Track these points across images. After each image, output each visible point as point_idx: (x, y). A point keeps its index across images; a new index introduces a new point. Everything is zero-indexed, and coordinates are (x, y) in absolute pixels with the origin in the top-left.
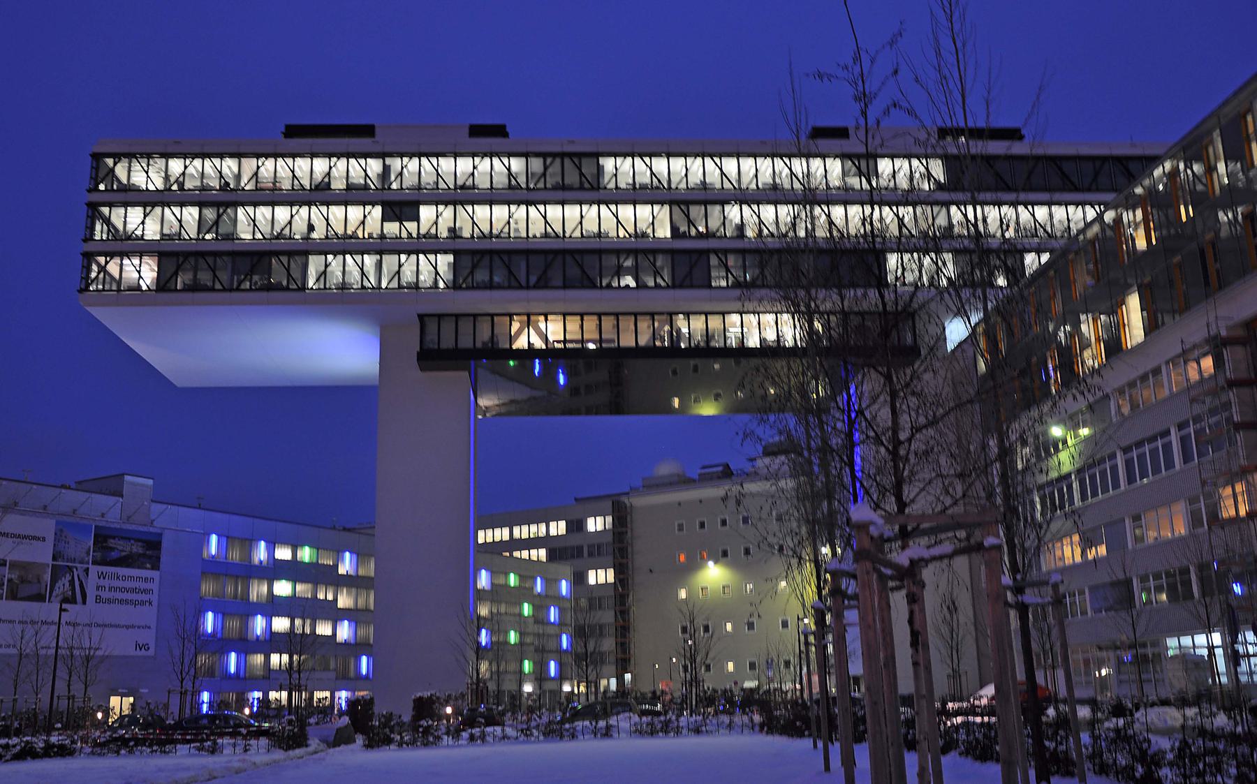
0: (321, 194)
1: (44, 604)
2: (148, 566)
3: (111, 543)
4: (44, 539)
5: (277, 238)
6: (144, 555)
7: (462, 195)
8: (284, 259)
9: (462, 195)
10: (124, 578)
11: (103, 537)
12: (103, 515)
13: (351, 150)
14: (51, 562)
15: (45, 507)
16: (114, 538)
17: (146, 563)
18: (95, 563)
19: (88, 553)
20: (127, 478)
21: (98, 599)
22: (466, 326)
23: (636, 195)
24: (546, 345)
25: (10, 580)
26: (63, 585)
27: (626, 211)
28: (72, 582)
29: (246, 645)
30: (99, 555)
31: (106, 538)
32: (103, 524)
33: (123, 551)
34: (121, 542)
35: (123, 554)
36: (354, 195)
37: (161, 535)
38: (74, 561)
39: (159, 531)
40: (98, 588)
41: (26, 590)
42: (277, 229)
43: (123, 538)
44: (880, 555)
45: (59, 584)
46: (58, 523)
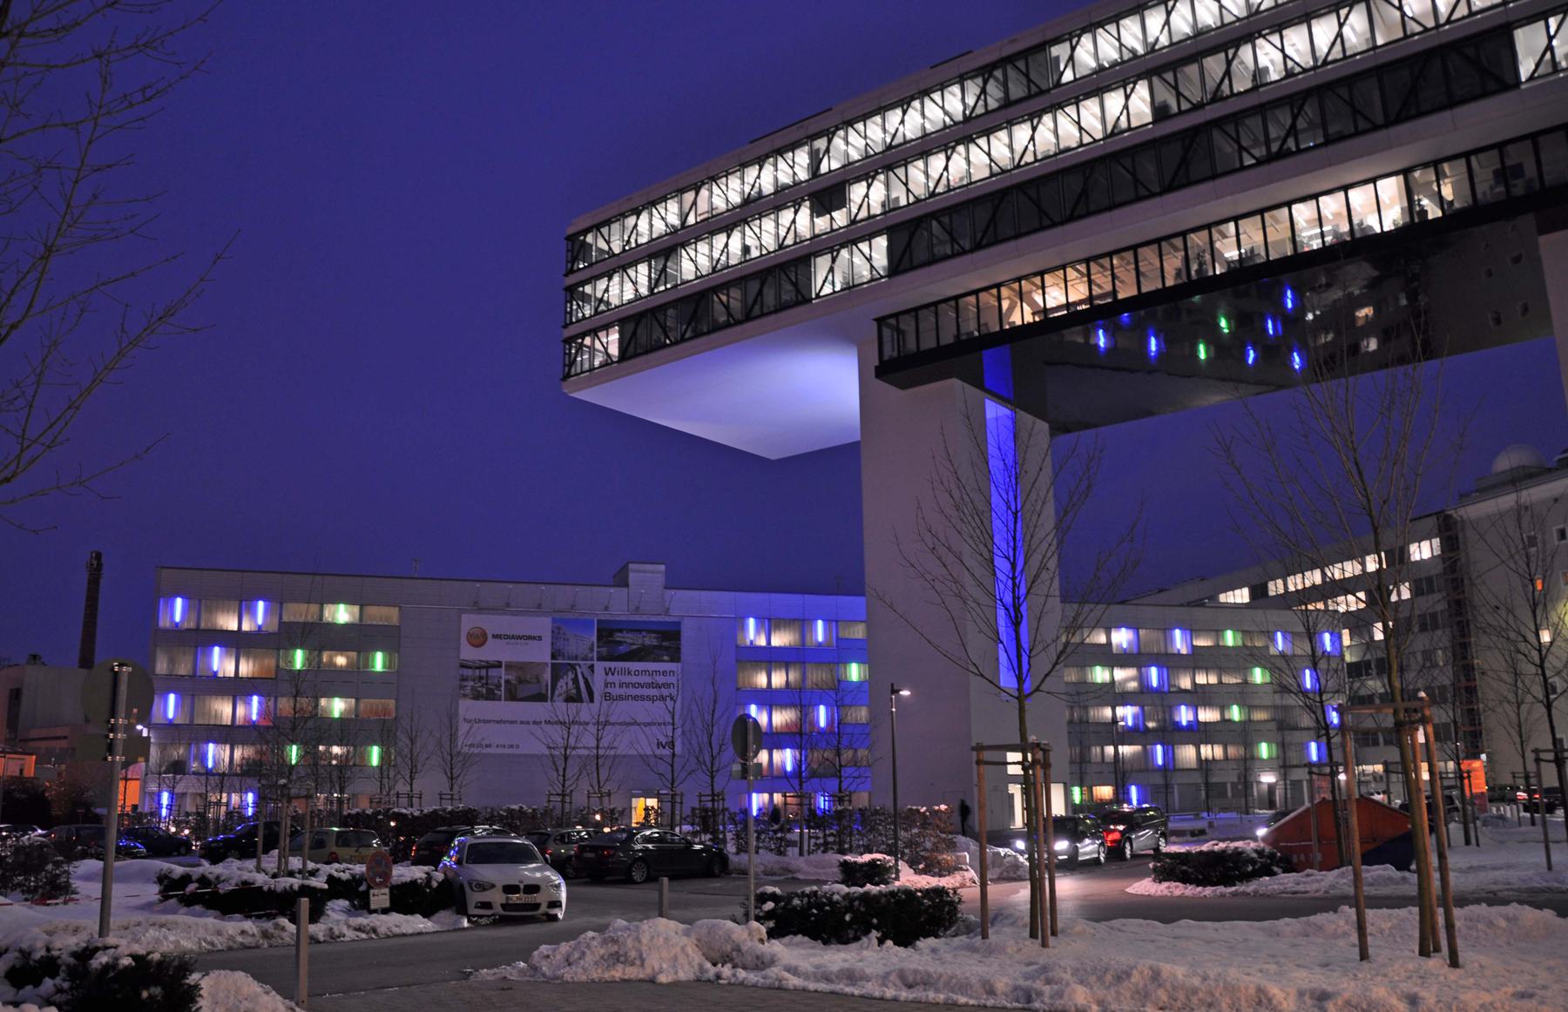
0: (752, 208)
1: (544, 704)
2: (666, 658)
3: (618, 637)
4: (540, 638)
5: (1113, 134)
6: (659, 647)
7: (893, 159)
8: (1127, 162)
9: (893, 159)
10: (637, 673)
11: (607, 632)
12: (606, 608)
13: (777, 145)
14: (548, 659)
15: (539, 606)
16: (621, 631)
17: (663, 655)
18: (599, 659)
19: (592, 650)
20: (631, 566)
21: (607, 697)
22: (928, 319)
23: (1098, 83)
24: (1442, 209)
25: (507, 682)
26: (565, 684)
27: (1090, 108)
28: (575, 680)
29: (1172, 734)
30: (604, 650)
31: (611, 632)
32: (608, 618)
33: (634, 644)
34: (630, 635)
35: (634, 647)
36: (784, 198)
37: (678, 624)
38: (576, 658)
39: (676, 620)
40: (606, 686)
41: (523, 691)
42: (1211, 85)
43: (632, 631)
44: (152, 740)
45: (561, 683)
46: (554, 621)
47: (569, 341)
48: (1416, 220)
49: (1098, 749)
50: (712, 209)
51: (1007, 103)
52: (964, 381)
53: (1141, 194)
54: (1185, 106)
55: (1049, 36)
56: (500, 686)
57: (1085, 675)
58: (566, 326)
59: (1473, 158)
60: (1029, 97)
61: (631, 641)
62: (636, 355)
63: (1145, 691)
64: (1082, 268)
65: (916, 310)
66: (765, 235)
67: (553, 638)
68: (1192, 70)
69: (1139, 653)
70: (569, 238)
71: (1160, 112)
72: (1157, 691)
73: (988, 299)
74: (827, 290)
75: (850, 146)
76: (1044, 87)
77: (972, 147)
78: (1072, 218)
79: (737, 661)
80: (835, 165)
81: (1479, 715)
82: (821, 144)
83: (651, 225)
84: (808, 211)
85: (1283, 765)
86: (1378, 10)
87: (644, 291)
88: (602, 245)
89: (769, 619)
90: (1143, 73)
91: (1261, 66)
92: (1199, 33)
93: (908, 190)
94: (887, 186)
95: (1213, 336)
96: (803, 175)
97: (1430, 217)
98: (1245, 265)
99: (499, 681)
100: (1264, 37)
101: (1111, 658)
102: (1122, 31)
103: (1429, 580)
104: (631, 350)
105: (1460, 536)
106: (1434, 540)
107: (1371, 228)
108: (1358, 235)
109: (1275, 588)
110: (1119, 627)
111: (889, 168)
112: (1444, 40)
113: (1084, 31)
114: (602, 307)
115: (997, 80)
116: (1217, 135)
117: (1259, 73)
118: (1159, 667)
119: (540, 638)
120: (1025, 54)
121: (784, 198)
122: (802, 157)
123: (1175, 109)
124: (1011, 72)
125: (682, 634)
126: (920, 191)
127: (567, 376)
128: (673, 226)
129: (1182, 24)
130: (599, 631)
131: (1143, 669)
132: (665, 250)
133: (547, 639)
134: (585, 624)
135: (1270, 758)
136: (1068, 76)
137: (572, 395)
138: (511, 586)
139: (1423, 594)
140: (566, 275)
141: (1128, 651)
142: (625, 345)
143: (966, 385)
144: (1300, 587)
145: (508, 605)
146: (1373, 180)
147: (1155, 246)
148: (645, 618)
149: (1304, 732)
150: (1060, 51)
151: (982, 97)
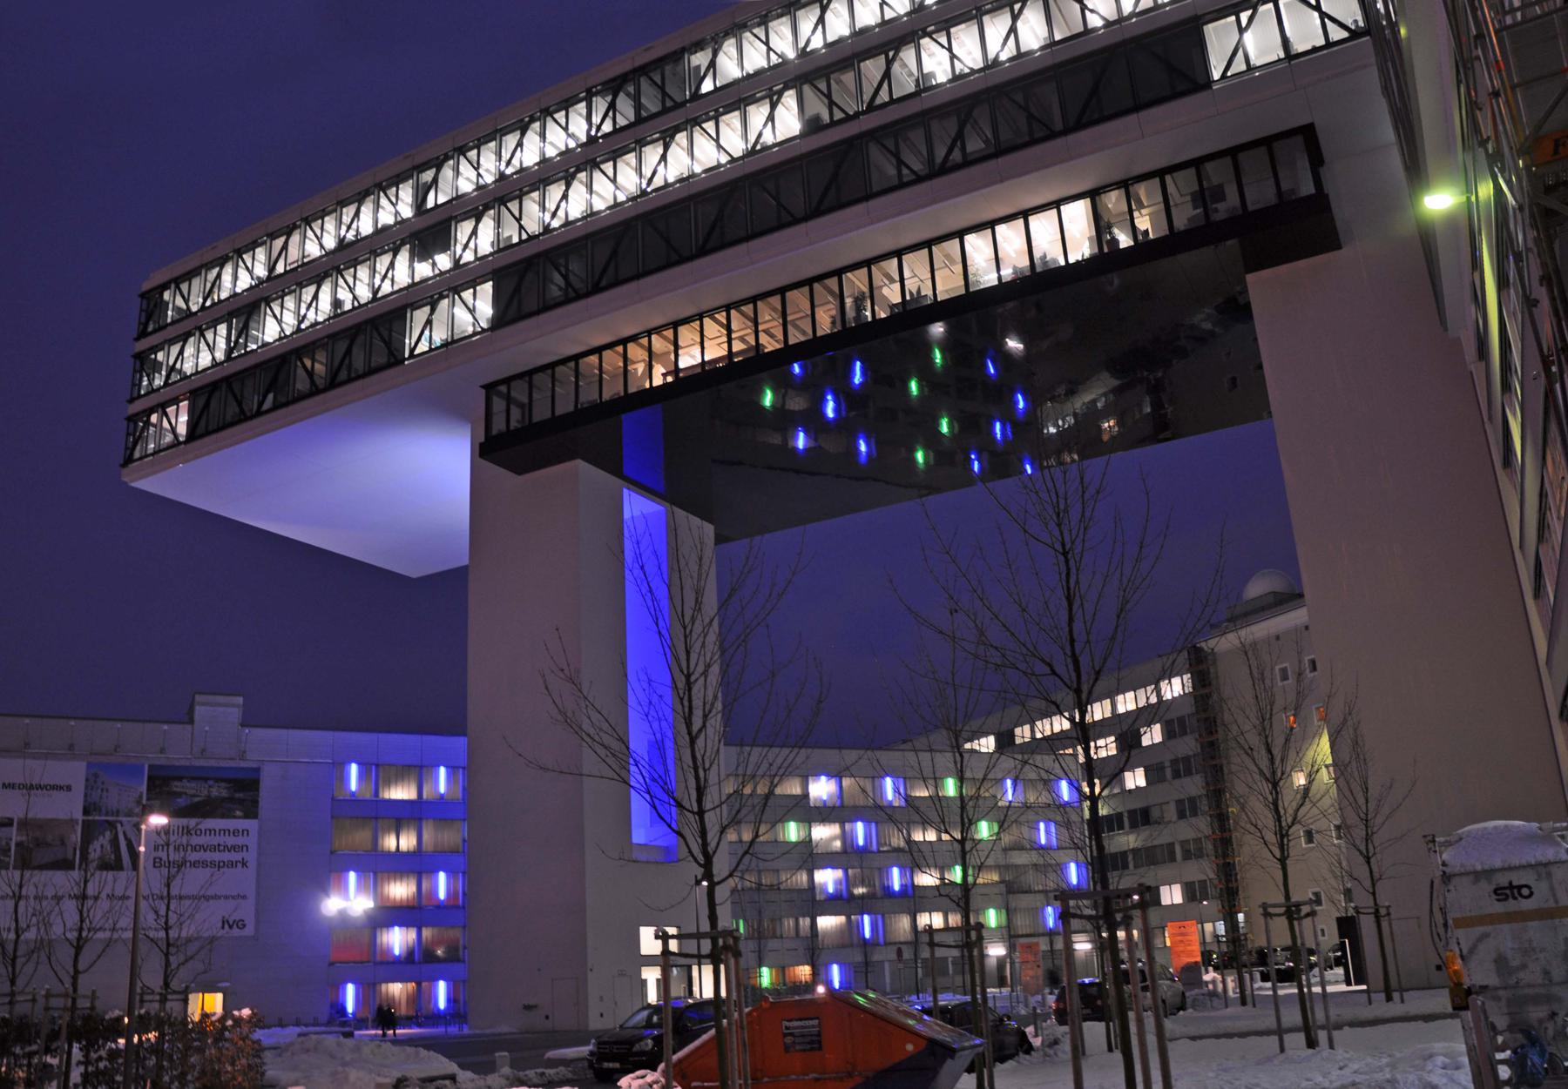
0: (348, 255)
2: (238, 813)
4: (69, 788)
6: (231, 799)
15: (71, 747)
16: (180, 779)
23: (738, 96)
31: (167, 780)
34: (193, 785)
35: (197, 799)
37: (257, 770)
39: (255, 766)
46: (90, 765)
47: (132, 419)
48: (1106, 250)
49: (792, 922)
50: (304, 257)
51: (639, 121)
52: (687, 511)
53: (786, 220)
54: (838, 115)
55: (686, 42)
56: (9, 850)
57: (776, 834)
58: (131, 401)
59: (1168, 178)
60: (665, 111)
61: (193, 792)
62: (208, 433)
63: (849, 850)
64: (722, 317)
65: (530, 373)
66: (359, 287)
67: (86, 788)
68: (848, 78)
69: (842, 806)
70: (143, 296)
71: (812, 126)
72: (864, 851)
73: (612, 359)
74: (423, 347)
75: (463, 179)
76: (679, 99)
77: (597, 175)
78: (703, 252)
79: (332, 817)
80: (442, 199)
81: (1236, 874)
82: (428, 176)
83: (237, 280)
84: (407, 255)
85: (1010, 935)
86: (1060, 11)
87: (220, 356)
88: (180, 302)
89: (377, 766)
90: (791, 80)
91: (926, 71)
92: (859, 34)
93: (521, 227)
94: (498, 223)
95: (933, 441)
96: (407, 212)
97: (1122, 246)
98: (908, 308)
99: (8, 844)
100: (930, 35)
101: (814, 813)
102: (772, 36)
103: (1181, 720)
104: (201, 429)
105: (1212, 670)
106: (1184, 676)
107: (1055, 261)
108: (1039, 269)
109: (1023, 734)
110: (817, 775)
111: (502, 201)
112: (1127, 35)
113: (727, 34)
114: (175, 377)
115: (628, 95)
116: (875, 152)
117: (923, 76)
118: (866, 821)
119: (69, 788)
120: (660, 62)
121: (384, 242)
122: (406, 193)
123: (826, 118)
124: (645, 84)
125: (262, 785)
126: (533, 227)
127: (129, 460)
128: (258, 278)
129: (838, 25)
130: (150, 778)
131: (847, 826)
132: (247, 309)
133: (79, 788)
134: (132, 771)
135: (999, 927)
136: (707, 86)
137: (133, 485)
138: (27, 721)
139: (1175, 737)
140: (137, 339)
141: (829, 804)
142: (195, 421)
143: (691, 516)
144: (1048, 733)
145: (27, 745)
146: (1057, 204)
147: (806, 289)
148: (213, 763)
149: (1037, 895)
150: (700, 59)
151: (611, 114)
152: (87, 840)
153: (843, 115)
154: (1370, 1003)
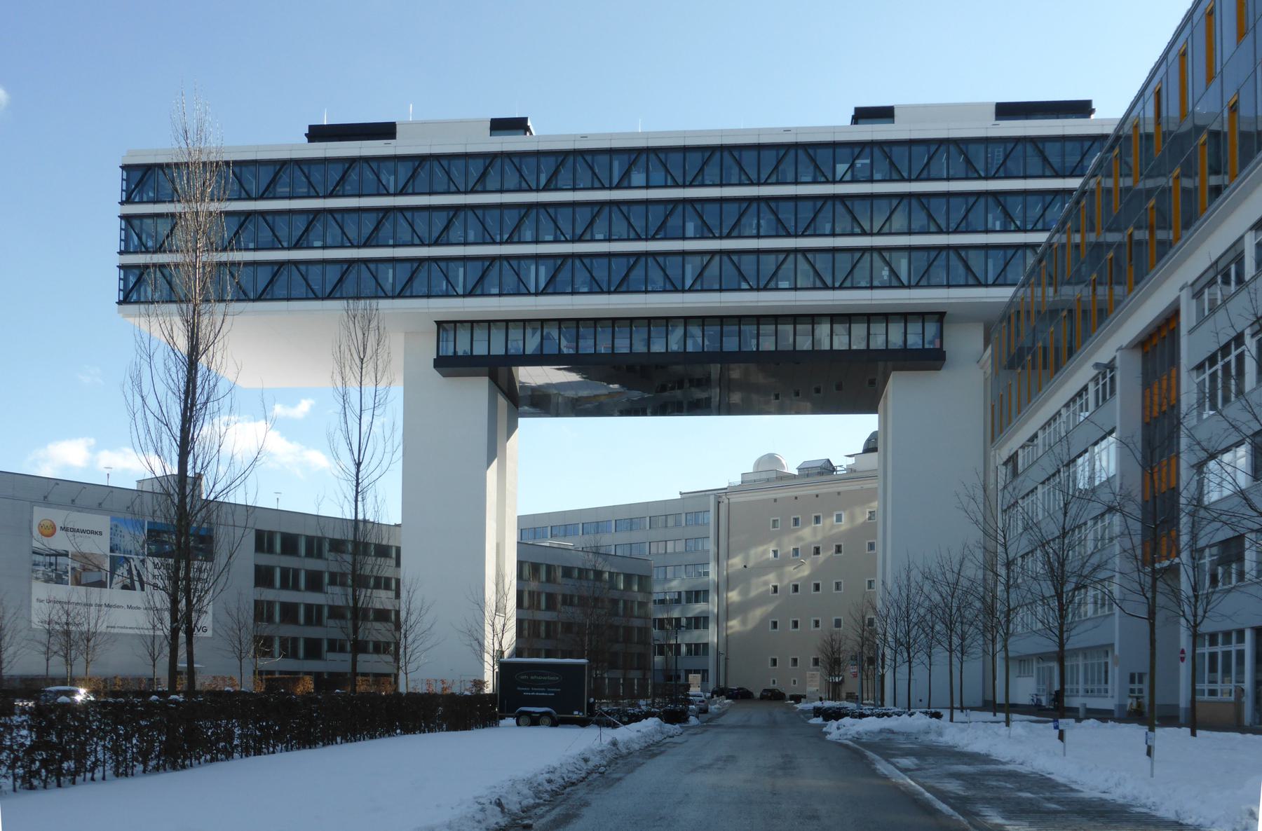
4: (101, 533)
67: (111, 534)
119: (101, 533)
152: (113, 572)
153: (477, 212)
154: (1065, 755)
